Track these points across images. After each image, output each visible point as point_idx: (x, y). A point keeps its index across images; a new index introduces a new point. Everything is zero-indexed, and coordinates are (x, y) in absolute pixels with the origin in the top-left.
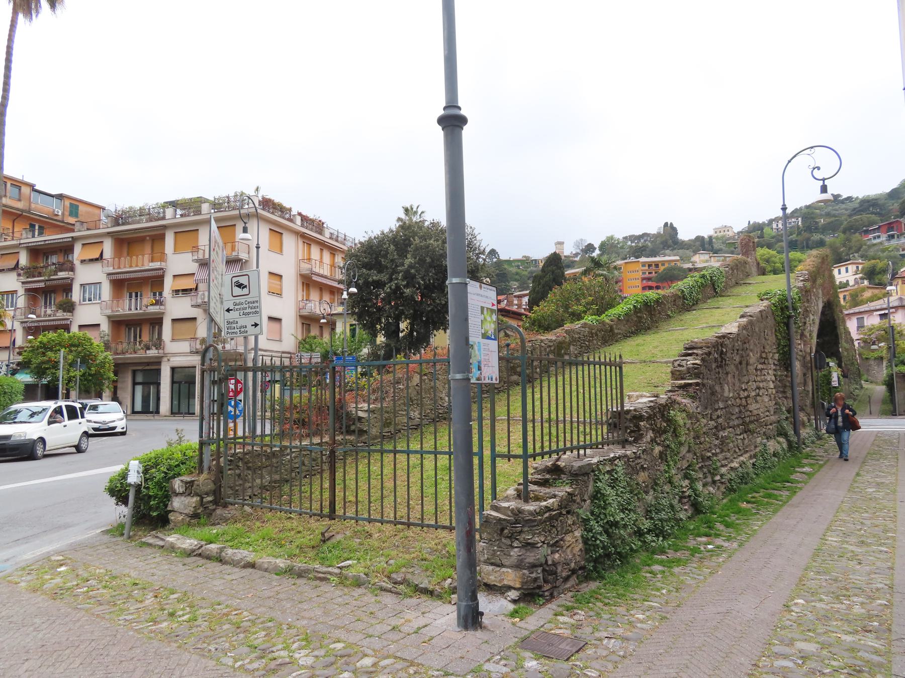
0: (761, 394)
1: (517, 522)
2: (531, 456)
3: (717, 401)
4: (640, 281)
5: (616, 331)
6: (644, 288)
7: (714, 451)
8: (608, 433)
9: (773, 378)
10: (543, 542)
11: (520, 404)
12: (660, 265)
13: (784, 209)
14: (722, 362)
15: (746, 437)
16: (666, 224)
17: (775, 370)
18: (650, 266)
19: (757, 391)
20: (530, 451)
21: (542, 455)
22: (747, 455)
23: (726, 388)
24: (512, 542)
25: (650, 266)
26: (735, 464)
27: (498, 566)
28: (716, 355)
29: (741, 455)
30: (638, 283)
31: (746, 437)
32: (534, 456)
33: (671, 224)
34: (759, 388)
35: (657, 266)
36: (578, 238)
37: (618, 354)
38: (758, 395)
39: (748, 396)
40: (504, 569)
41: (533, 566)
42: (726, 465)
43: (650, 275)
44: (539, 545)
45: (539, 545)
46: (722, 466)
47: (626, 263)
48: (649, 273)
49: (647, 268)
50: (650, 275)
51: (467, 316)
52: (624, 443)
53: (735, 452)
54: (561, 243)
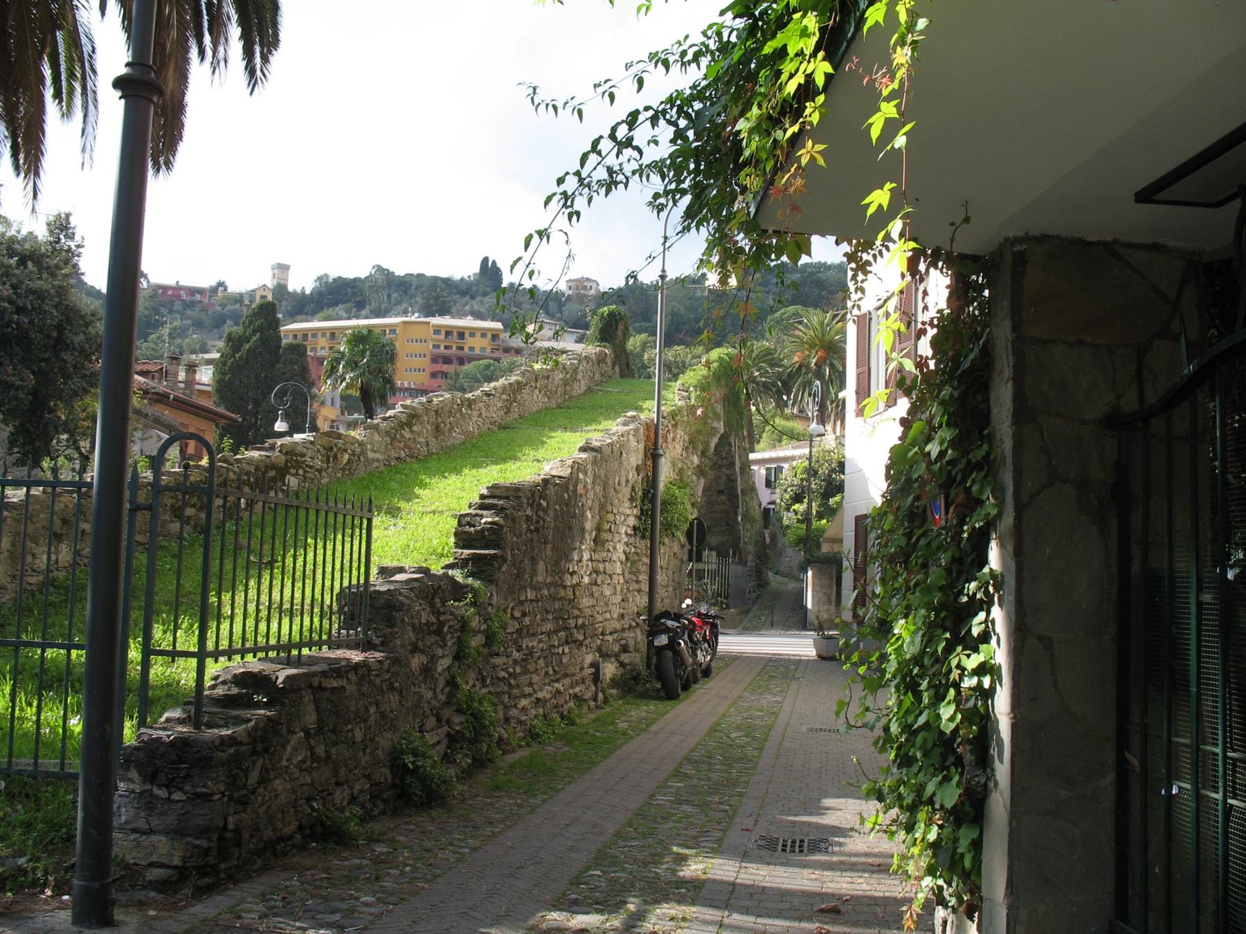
0: (599, 582)
1: (181, 760)
2: (211, 654)
3: (524, 588)
4: (427, 360)
5: (370, 455)
6: (434, 375)
7: (511, 670)
8: (339, 628)
9: (623, 557)
10: (223, 793)
11: (200, 561)
12: (467, 335)
13: (663, 277)
14: (538, 522)
15: (567, 650)
16: (486, 260)
17: (627, 544)
18: (448, 333)
19: (594, 575)
20: (210, 645)
21: (229, 653)
22: (567, 681)
23: (541, 566)
24: (170, 794)
25: (448, 333)
26: (544, 694)
27: (144, 833)
28: (529, 512)
29: (557, 681)
30: (425, 362)
31: (567, 650)
32: (216, 655)
33: (494, 262)
34: (597, 572)
35: (461, 335)
36: (320, 273)
37: (341, 496)
38: (596, 584)
39: (578, 584)
40: (153, 838)
41: (204, 831)
42: (530, 695)
43: (448, 352)
44: (217, 797)
45: (217, 797)
46: (524, 696)
47: (405, 323)
48: (447, 347)
49: (442, 336)
50: (448, 352)
51: (1009, 837)
52: (367, 646)
53: (547, 673)
54: (283, 268)
